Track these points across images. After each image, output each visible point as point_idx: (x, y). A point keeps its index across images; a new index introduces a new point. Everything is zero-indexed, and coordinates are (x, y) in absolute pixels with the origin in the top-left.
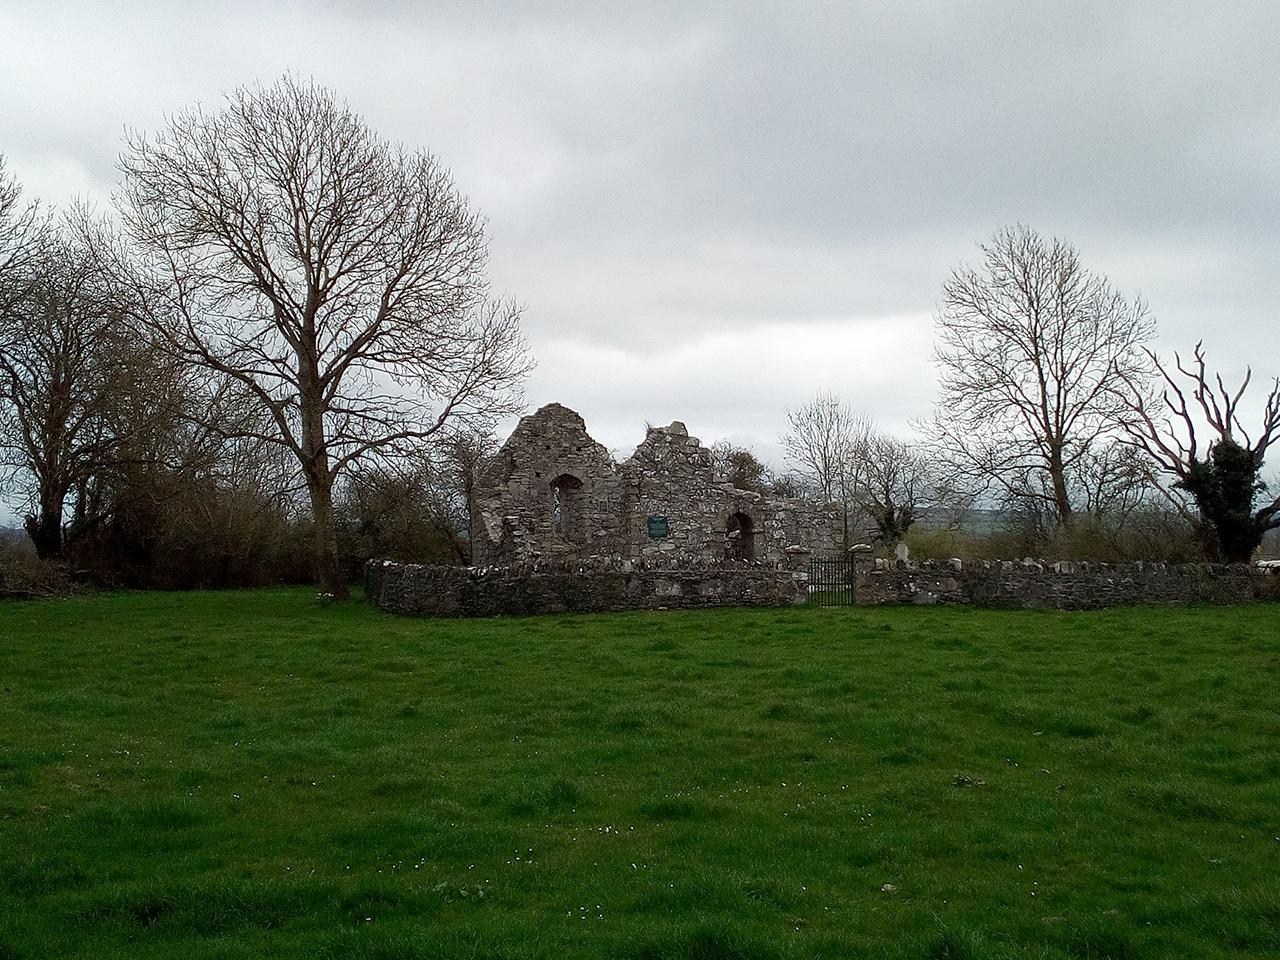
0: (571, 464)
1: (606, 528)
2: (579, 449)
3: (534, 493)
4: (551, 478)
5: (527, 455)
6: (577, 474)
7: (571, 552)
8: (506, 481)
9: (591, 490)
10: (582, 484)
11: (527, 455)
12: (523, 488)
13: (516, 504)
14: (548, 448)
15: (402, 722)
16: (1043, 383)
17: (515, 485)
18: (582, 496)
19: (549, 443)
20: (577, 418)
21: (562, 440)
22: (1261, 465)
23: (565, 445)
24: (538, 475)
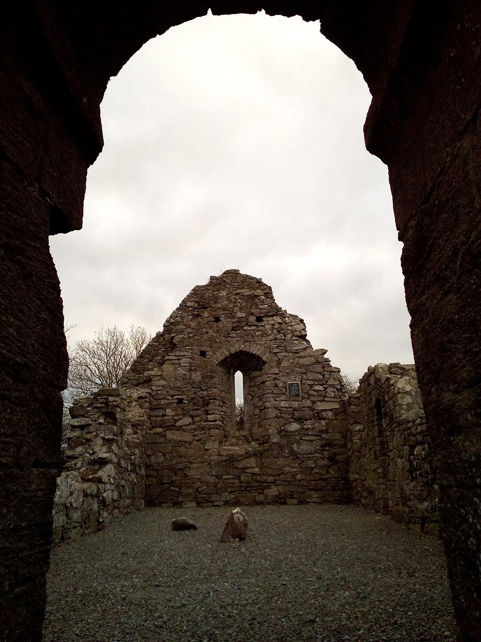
0: (248, 338)
1: (300, 420)
2: (259, 319)
3: (197, 376)
4: (220, 356)
5: (190, 330)
6: (255, 350)
7: (248, 455)
8: (161, 364)
9: (276, 370)
10: (264, 363)
11: (190, 330)
12: (181, 371)
13: (171, 392)
14: (217, 320)
15: (398, 496)
16: (334, 402)
17: (171, 368)
18: (264, 378)
19: (219, 313)
20: (232, 275)
21: (235, 309)
22: (212, 278)
23: (239, 315)
24: (203, 354)
